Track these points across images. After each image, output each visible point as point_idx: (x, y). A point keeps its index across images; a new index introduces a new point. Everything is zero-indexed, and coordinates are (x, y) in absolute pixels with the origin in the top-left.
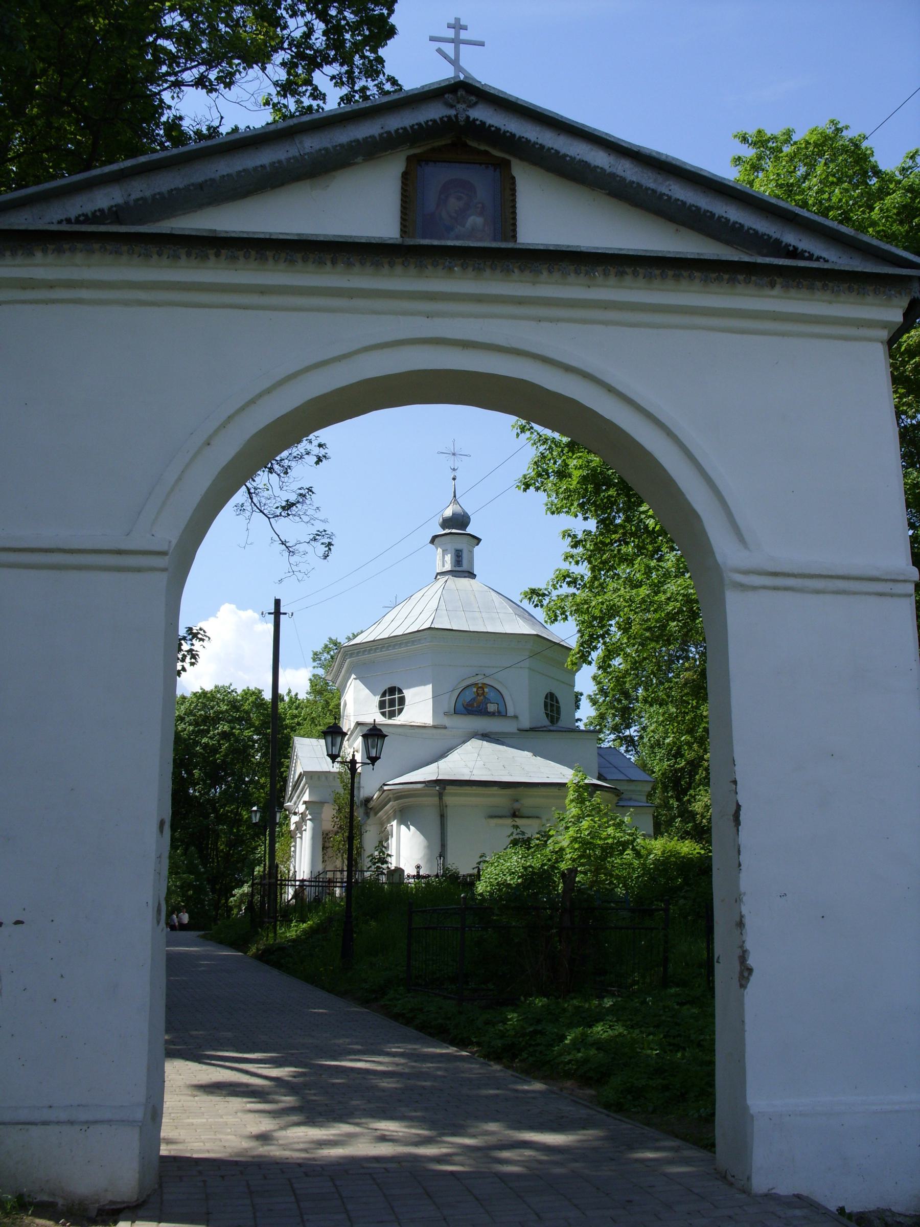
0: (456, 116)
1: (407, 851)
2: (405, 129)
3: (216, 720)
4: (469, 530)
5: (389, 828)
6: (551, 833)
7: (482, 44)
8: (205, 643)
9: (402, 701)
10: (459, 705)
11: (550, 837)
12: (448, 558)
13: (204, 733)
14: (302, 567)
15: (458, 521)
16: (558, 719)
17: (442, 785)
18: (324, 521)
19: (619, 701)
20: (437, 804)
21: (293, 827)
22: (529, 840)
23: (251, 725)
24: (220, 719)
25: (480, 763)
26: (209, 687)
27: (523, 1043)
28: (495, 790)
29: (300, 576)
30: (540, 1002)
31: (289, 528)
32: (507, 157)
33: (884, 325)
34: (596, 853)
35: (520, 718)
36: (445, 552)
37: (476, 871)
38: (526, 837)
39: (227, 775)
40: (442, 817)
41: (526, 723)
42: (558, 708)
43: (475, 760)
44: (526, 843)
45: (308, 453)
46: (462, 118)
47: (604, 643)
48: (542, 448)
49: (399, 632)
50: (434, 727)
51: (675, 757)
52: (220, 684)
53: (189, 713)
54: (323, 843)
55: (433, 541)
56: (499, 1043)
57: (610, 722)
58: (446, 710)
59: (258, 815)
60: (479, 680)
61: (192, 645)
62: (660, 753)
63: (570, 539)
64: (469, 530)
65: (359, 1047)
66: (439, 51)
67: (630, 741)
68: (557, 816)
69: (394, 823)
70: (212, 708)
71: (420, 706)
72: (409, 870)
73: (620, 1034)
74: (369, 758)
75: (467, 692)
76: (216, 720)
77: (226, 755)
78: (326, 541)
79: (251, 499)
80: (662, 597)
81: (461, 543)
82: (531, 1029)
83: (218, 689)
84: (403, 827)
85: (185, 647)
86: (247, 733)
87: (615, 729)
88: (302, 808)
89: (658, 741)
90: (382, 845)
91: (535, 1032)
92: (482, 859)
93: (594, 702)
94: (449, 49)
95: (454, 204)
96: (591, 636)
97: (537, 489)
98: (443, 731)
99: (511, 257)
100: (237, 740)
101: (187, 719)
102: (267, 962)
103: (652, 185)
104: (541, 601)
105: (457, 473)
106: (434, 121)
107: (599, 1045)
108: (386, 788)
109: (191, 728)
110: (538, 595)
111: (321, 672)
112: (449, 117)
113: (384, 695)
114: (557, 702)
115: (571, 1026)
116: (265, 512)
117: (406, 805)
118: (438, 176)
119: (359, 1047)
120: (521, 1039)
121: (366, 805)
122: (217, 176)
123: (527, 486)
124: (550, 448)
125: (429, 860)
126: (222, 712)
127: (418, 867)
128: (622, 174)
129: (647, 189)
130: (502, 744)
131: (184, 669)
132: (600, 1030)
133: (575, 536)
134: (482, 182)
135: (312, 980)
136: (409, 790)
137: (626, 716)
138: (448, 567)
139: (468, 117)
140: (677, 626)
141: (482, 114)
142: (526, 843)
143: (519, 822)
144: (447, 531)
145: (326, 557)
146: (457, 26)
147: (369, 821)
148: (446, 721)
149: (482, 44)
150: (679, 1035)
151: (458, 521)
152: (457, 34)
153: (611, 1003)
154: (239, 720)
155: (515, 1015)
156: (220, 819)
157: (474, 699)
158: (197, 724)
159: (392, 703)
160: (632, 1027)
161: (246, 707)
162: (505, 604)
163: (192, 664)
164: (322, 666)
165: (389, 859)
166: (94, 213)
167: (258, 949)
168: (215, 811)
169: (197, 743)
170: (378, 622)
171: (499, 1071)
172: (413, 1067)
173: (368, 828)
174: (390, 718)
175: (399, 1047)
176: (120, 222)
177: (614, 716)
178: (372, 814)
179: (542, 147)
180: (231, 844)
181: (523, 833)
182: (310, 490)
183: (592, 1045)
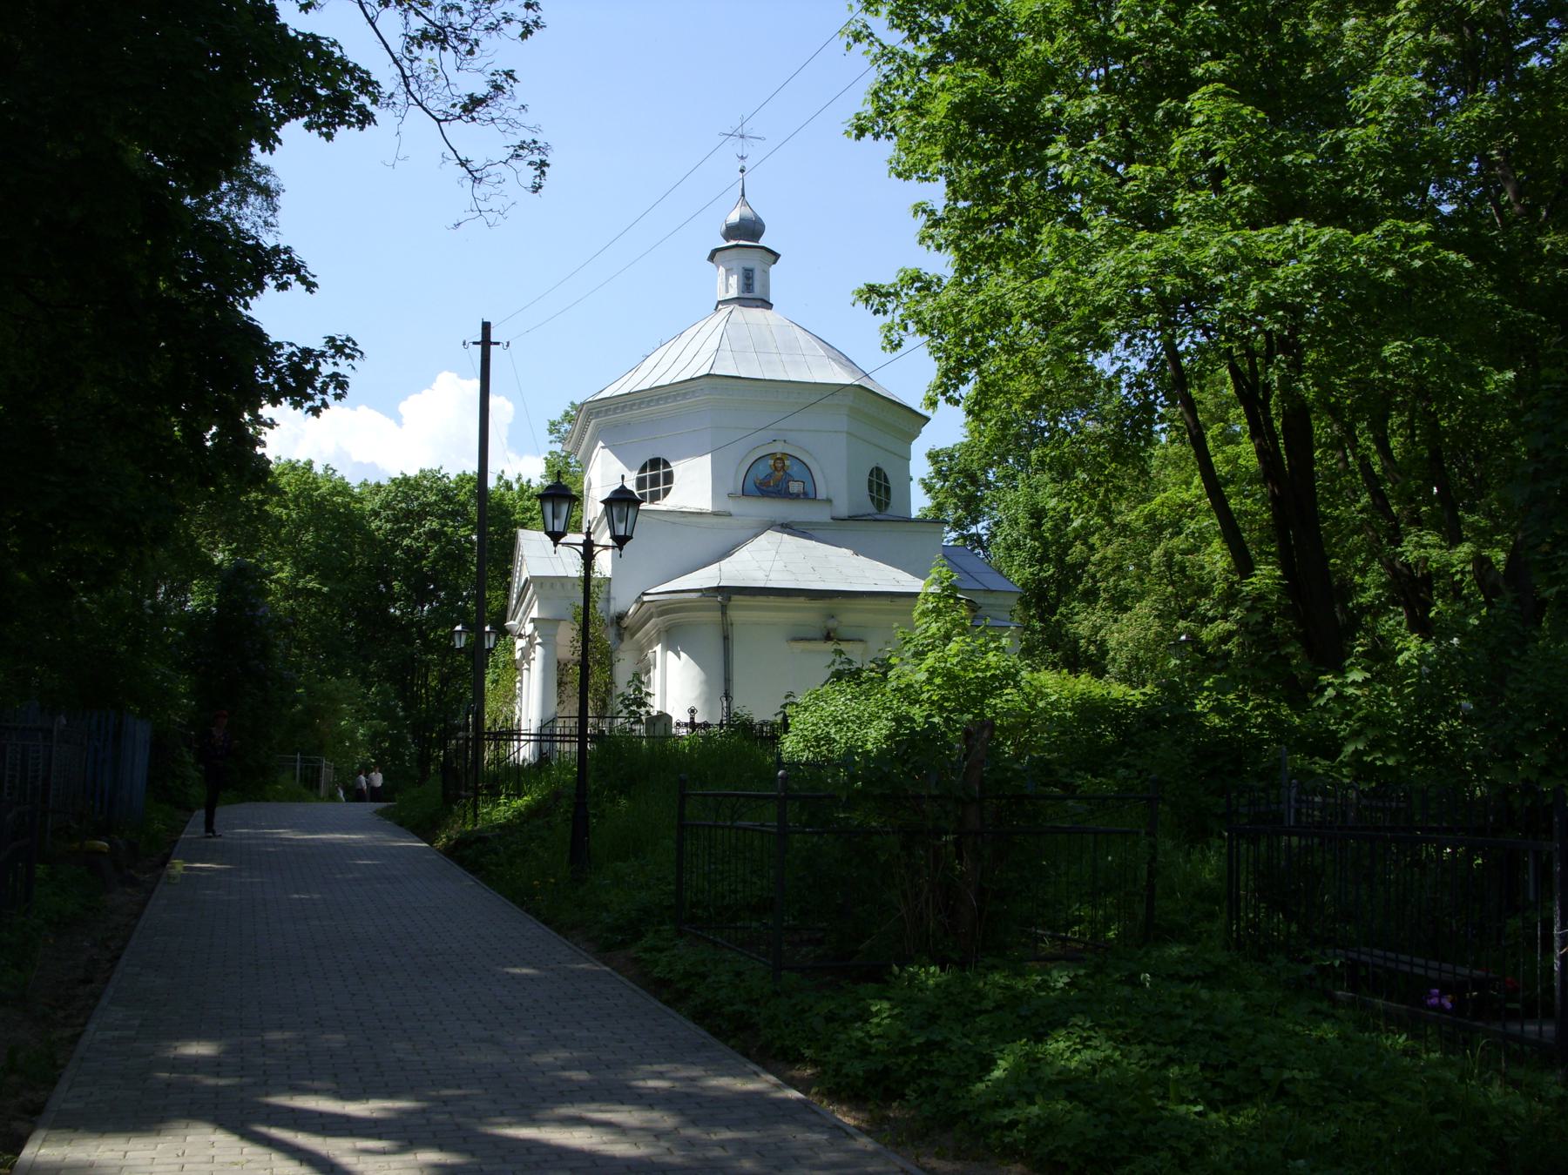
1: (676, 688)
3: (421, 515)
4: (762, 242)
5: (650, 655)
6: (893, 661)
8: (356, 363)
9: (669, 478)
10: (750, 485)
11: (891, 667)
12: (734, 280)
13: (406, 532)
14: (495, 203)
15: (747, 231)
16: (887, 504)
17: (725, 593)
18: (536, 129)
19: (963, 487)
20: (718, 622)
21: (518, 655)
22: (859, 671)
23: (469, 521)
24: (427, 513)
25: (779, 565)
26: (413, 472)
27: (906, 1068)
28: (801, 602)
29: (491, 217)
30: (932, 976)
31: (480, 140)
34: (964, 690)
35: (835, 502)
36: (729, 272)
37: (779, 719)
38: (853, 668)
39: (437, 589)
40: (726, 639)
41: (843, 510)
42: (888, 490)
43: (771, 560)
44: (855, 675)
45: (508, 20)
47: (980, 373)
48: (886, 69)
49: (665, 381)
50: (714, 514)
51: (1041, 561)
52: (427, 467)
53: (387, 505)
54: (558, 675)
55: (712, 258)
56: (857, 1068)
57: (951, 514)
58: (731, 490)
59: (464, 637)
60: (778, 448)
61: (335, 364)
62: (1020, 556)
63: (925, 217)
64: (762, 242)
65: (580, 1076)
67: (977, 540)
68: (900, 636)
69: (658, 648)
70: (417, 498)
71: (694, 485)
72: (679, 715)
73: (1106, 1060)
76: (421, 515)
77: (435, 562)
78: (536, 158)
79: (407, 85)
80: (1090, 284)
81: (753, 260)
82: (921, 1040)
83: (424, 474)
84: (670, 654)
85: (326, 369)
86: (462, 532)
87: (958, 524)
88: (529, 628)
89: (1017, 540)
90: (639, 679)
91: (930, 1045)
92: (789, 700)
93: (929, 488)
96: (959, 360)
97: (877, 136)
98: (726, 520)
100: (450, 542)
101: (383, 514)
102: (461, 862)
104: (884, 305)
105: (748, 164)
107: (1071, 1086)
108: (646, 598)
109: (389, 526)
110: (880, 295)
111: (558, 447)
113: (643, 469)
114: (886, 480)
115: (1004, 1035)
116: (430, 104)
117: (676, 623)
119: (580, 1076)
120: (901, 1060)
121: (618, 624)
123: (861, 132)
124: (899, 69)
125: (708, 700)
126: (429, 504)
127: (692, 711)
130: (810, 538)
131: (325, 404)
132: (1063, 1051)
133: (933, 212)
135: (522, 898)
136: (680, 601)
137: (972, 508)
138: (733, 293)
140: (1117, 326)
142: (855, 675)
143: (844, 646)
144: (733, 243)
145: (537, 188)
147: (623, 646)
148: (731, 506)
150: (1232, 1065)
151: (747, 231)
153: (1066, 980)
154: (453, 515)
155: (886, 1005)
156: (429, 646)
157: (770, 475)
158: (396, 520)
159: (655, 481)
160: (1126, 1040)
161: (462, 498)
162: (814, 343)
163: (338, 397)
164: (562, 440)
165: (650, 700)
167: (449, 838)
168: (423, 635)
169: (396, 546)
170: (635, 369)
171: (875, 1154)
172: (690, 1143)
173: (621, 656)
174: (652, 501)
175: (660, 1075)
177: (957, 508)
178: (626, 636)
180: (444, 680)
181: (850, 662)
182: (509, 74)
183: (1053, 1085)
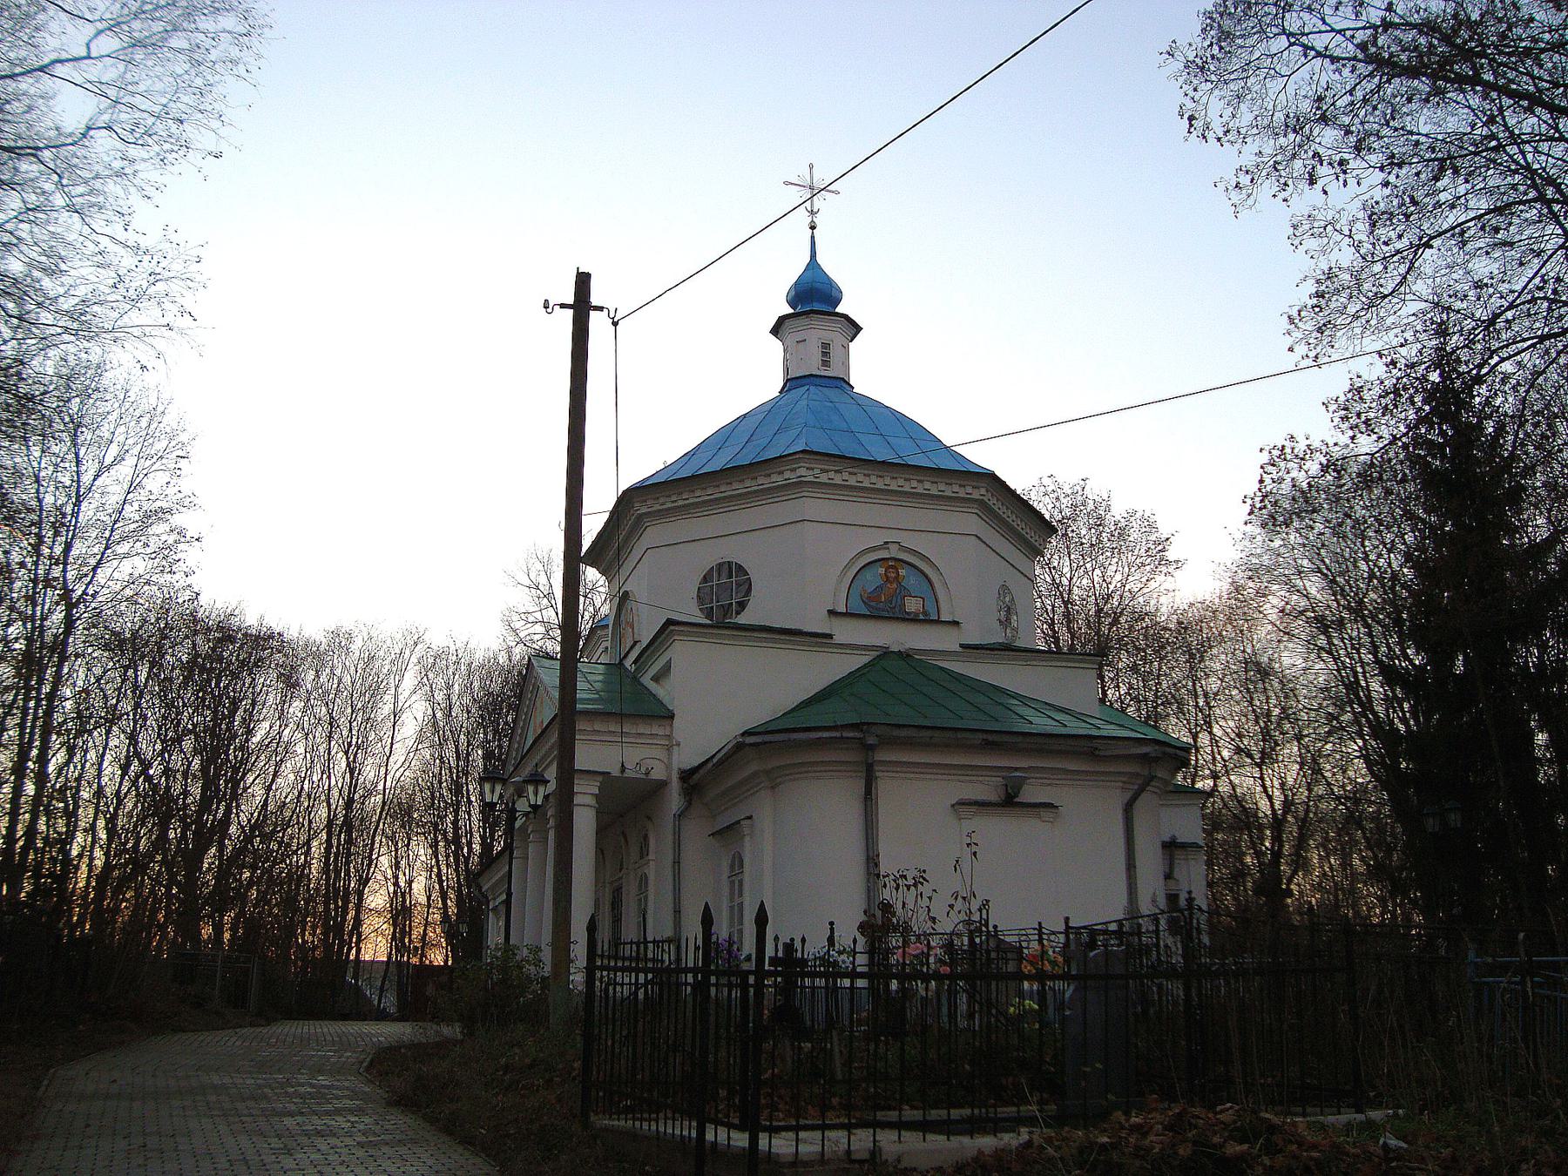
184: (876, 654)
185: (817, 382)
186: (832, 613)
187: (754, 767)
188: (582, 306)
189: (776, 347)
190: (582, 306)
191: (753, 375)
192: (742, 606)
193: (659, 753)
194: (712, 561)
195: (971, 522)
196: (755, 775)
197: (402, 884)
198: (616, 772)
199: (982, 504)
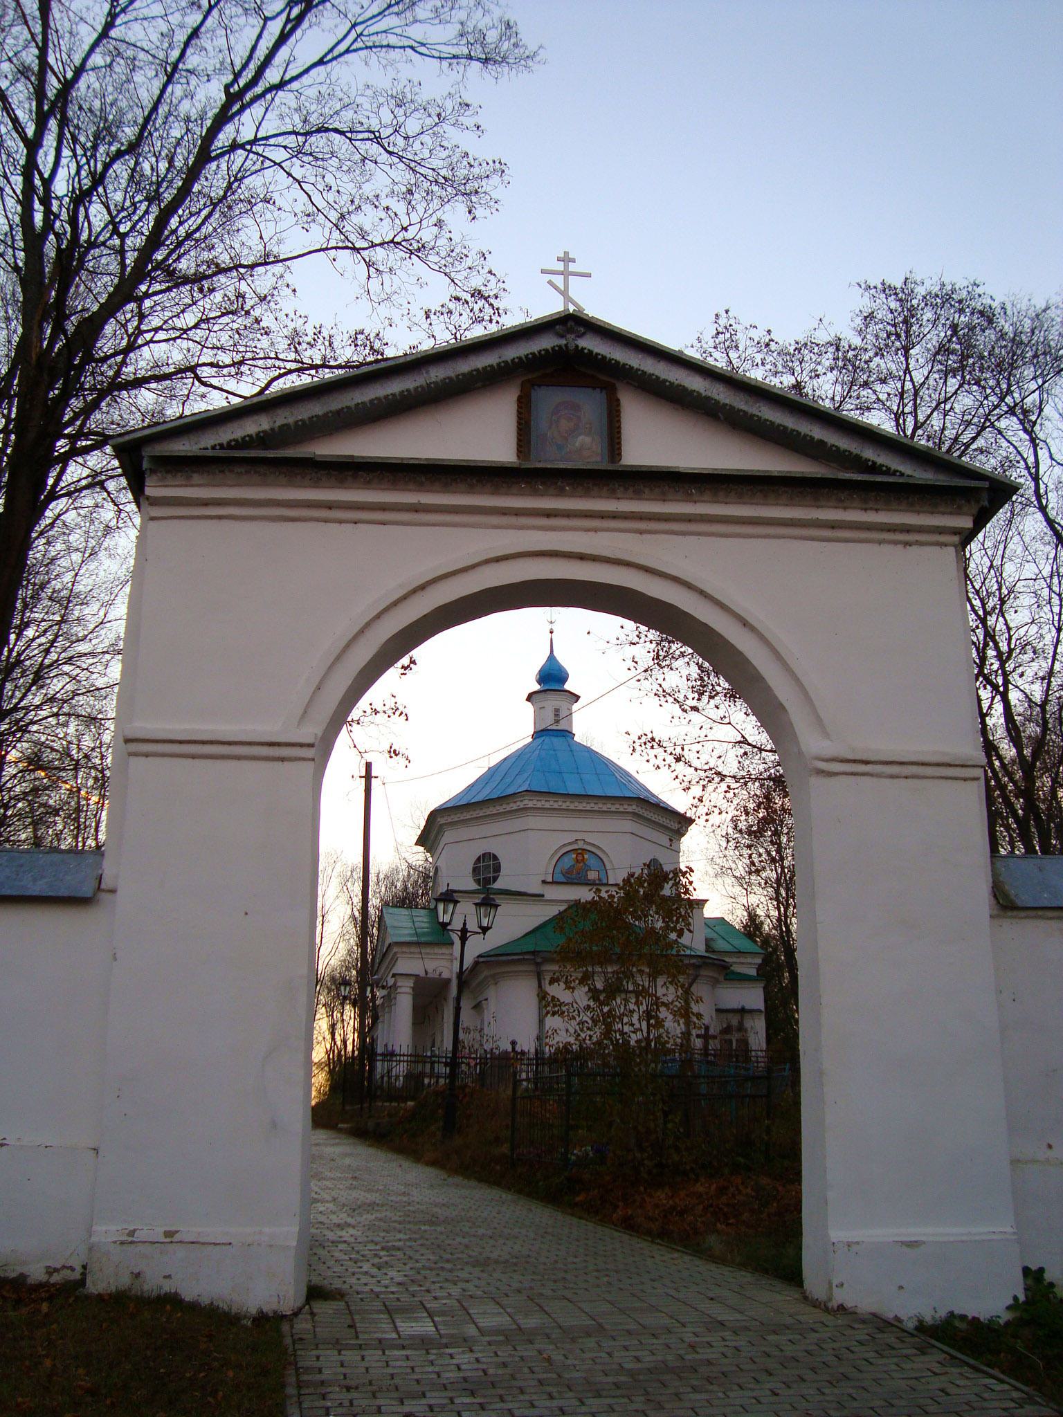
0: (566, 345)
2: (520, 358)
4: (567, 686)
7: (589, 275)
32: (613, 381)
33: (955, 531)
46: (572, 347)
64: (567, 686)
66: (550, 283)
74: (481, 927)
75: (566, 859)
94: (559, 280)
95: (565, 425)
99: (619, 478)
103: (743, 407)
105: (554, 627)
106: (546, 350)
112: (560, 347)
118: (549, 399)
122: (352, 404)
128: (717, 397)
129: (739, 410)
134: (589, 404)
139: (577, 346)
141: (590, 344)
146: (566, 259)
149: (589, 275)
152: (566, 267)
166: (243, 438)
176: (266, 448)
179: (644, 373)
184: (562, 908)
185: (553, 733)
186: (544, 882)
187: (486, 973)
188: (368, 777)
189: (529, 709)
190: (368, 777)
191: (515, 728)
192: (495, 879)
193: (447, 964)
194: (479, 853)
195: (628, 825)
196: (486, 977)
197: (339, 1043)
198: (422, 974)
199: (634, 814)
